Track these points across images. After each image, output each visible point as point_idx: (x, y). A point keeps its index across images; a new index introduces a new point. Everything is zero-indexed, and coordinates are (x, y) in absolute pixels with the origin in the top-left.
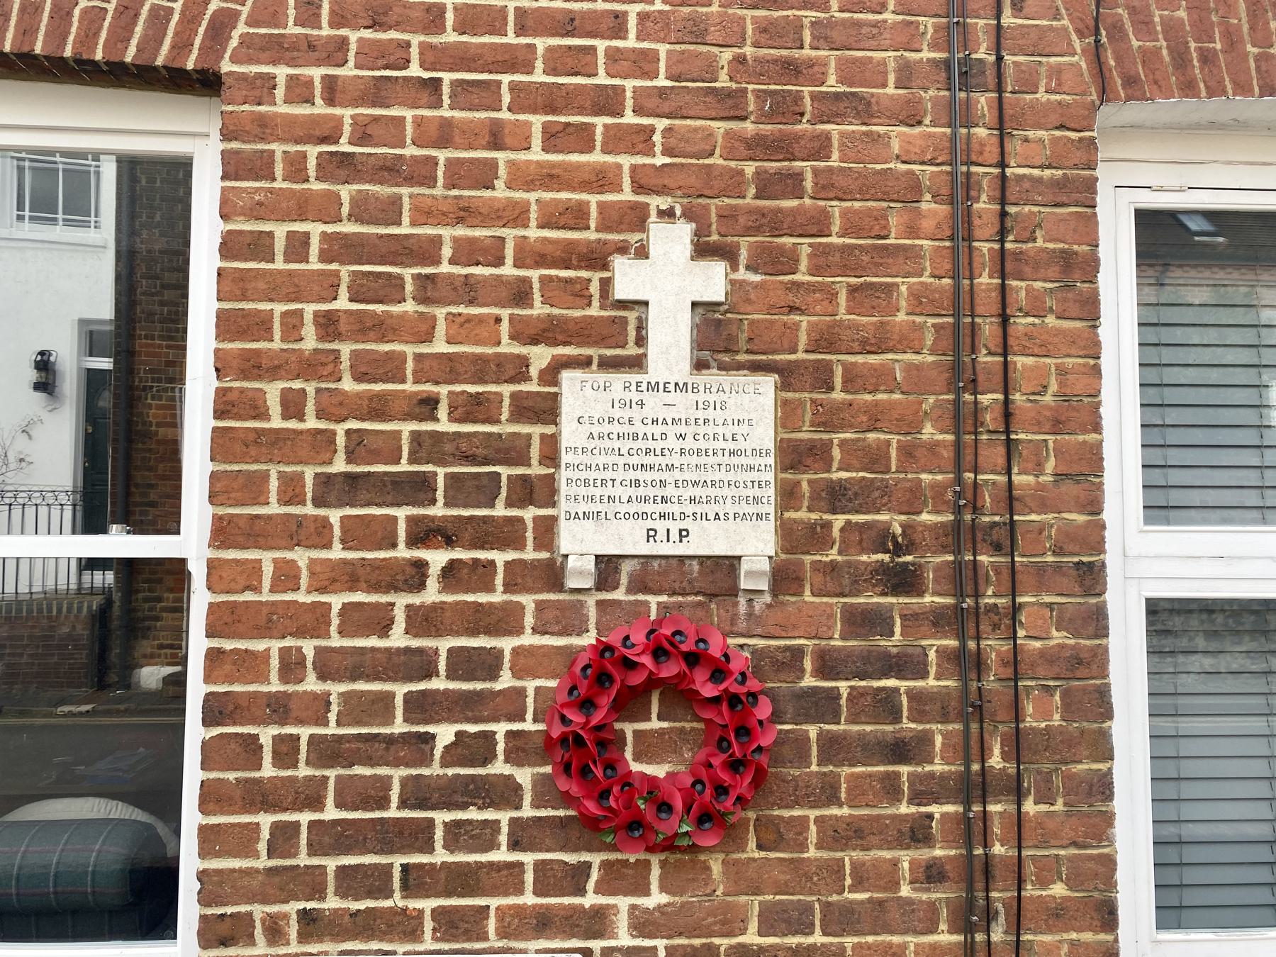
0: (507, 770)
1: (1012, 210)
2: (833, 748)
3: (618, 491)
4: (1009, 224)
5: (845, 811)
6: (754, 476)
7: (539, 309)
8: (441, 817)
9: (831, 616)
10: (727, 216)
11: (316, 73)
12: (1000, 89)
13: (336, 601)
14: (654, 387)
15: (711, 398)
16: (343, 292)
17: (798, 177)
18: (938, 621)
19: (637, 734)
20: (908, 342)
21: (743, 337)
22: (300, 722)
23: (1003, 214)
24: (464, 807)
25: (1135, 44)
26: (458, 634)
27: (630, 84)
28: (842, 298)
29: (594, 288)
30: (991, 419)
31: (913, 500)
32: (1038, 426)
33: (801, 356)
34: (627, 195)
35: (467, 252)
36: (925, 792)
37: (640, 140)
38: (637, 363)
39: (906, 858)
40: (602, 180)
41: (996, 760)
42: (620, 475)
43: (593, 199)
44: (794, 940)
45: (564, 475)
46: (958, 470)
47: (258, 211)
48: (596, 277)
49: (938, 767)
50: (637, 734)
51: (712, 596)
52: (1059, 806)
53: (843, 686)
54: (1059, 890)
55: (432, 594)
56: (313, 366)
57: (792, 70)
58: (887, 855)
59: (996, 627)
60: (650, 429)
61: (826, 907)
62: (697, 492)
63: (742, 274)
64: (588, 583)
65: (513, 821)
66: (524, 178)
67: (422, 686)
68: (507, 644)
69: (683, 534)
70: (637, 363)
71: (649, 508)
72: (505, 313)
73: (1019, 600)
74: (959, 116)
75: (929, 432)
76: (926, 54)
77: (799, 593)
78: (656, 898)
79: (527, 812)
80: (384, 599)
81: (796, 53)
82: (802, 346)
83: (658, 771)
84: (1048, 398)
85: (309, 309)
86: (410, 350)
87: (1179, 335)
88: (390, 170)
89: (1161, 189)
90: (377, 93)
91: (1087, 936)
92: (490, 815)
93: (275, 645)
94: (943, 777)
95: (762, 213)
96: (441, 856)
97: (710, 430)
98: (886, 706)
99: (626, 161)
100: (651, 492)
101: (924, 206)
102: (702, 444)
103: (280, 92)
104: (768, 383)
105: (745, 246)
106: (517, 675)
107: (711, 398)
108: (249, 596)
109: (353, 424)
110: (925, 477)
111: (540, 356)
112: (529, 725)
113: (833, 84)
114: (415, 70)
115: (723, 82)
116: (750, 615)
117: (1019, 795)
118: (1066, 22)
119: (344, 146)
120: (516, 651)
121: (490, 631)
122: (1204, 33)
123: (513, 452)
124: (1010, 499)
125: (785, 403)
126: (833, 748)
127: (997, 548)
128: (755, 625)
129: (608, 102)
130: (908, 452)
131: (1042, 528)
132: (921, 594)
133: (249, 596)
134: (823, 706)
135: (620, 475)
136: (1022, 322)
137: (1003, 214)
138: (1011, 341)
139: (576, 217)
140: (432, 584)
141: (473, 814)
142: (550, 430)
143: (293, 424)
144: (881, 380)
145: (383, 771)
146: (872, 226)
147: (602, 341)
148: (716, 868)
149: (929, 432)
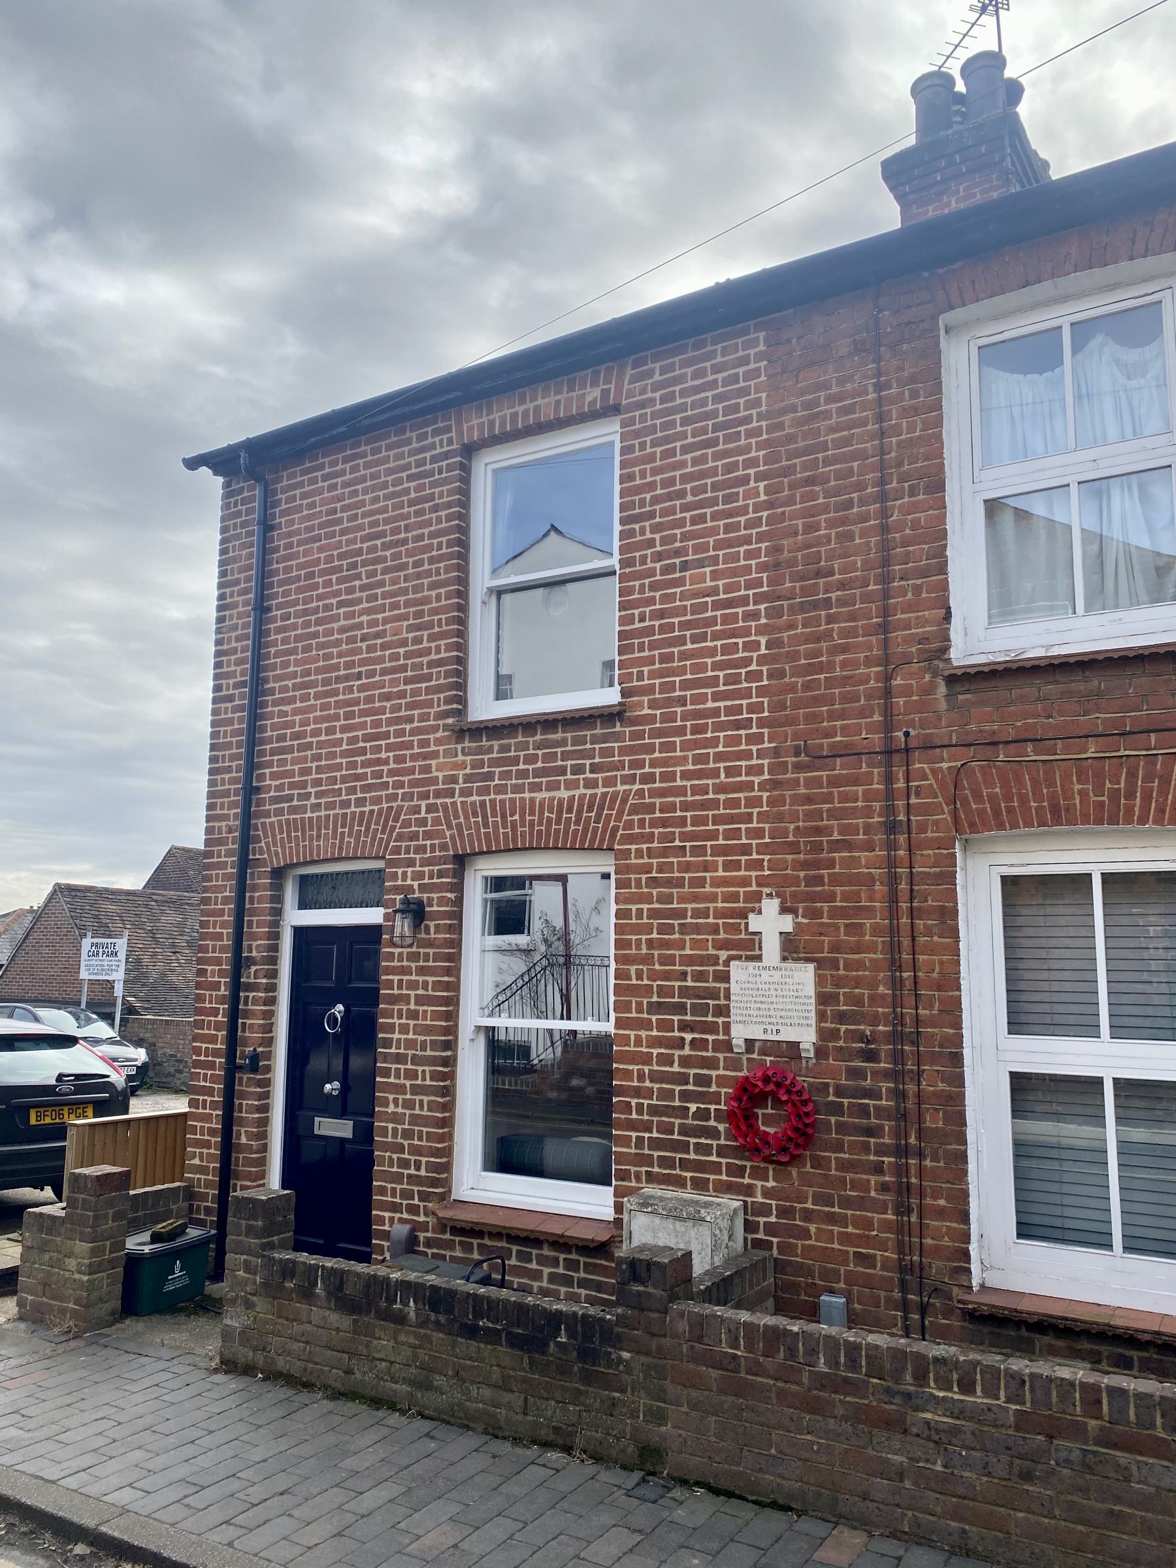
0: (715, 1124)
1: (916, 888)
2: (842, 1128)
3: (752, 1012)
4: (915, 894)
5: (847, 1156)
6: (806, 1007)
7: (722, 936)
8: (693, 1140)
9: (841, 1070)
10: (794, 895)
11: (644, 846)
12: (909, 833)
13: (655, 1052)
14: (765, 968)
15: (788, 973)
16: (655, 931)
17: (822, 877)
18: (886, 1075)
19: (763, 1114)
20: (871, 948)
21: (801, 946)
22: (644, 1098)
23: (912, 890)
24: (700, 1137)
25: (974, 806)
26: (696, 1068)
27: (754, 842)
28: (842, 929)
29: (742, 927)
30: (908, 984)
31: (874, 1020)
32: (930, 988)
33: (825, 955)
34: (754, 888)
35: (697, 914)
36: (881, 1150)
37: (757, 865)
38: (759, 958)
39: (873, 1179)
40: (745, 882)
41: (912, 1140)
42: (753, 1005)
43: (742, 890)
44: (827, 1209)
45: (732, 1005)
46: (894, 1008)
47: (628, 900)
48: (743, 922)
49: (887, 1140)
50: (763, 1114)
51: (792, 1059)
52: (942, 1164)
53: (846, 1101)
54: (942, 1202)
55: (687, 1051)
56: (647, 960)
57: (818, 831)
58: (864, 1177)
59: (912, 1079)
60: (764, 986)
61: (839, 1196)
62: (783, 1013)
63: (800, 919)
64: (743, 1050)
65: (718, 1145)
66: (717, 883)
67: (685, 1088)
68: (714, 1073)
69: (778, 1031)
70: (759, 958)
71: (764, 1020)
72: (710, 937)
73: (923, 1068)
74: (891, 846)
75: (881, 989)
76: (876, 819)
77: (827, 1059)
78: (771, 1184)
79: (723, 1142)
80: (671, 1052)
81: (820, 823)
82: (826, 949)
83: (771, 1130)
84: (935, 975)
85: (644, 937)
86: (677, 953)
87: (1054, 942)
88: (669, 883)
89: (1012, 865)
90: (665, 852)
91: (955, 1225)
92: (709, 1142)
93: (636, 1067)
94: (888, 1145)
95: (807, 893)
96: (692, 1156)
97: (787, 987)
98: (864, 1111)
99: (753, 874)
100: (765, 1013)
101: (876, 888)
102: (785, 993)
103: (633, 855)
104: (811, 967)
105: (801, 908)
106: (718, 1086)
107: (788, 973)
108: (627, 1048)
109: (659, 983)
110: (880, 1010)
111: (723, 955)
112: (723, 1107)
113: (836, 836)
114: (677, 843)
115: (791, 838)
116: (807, 1068)
117: (921, 1155)
118: (940, 799)
119: (654, 875)
120: (717, 1076)
121: (709, 1068)
122: (1008, 798)
123: (714, 994)
124: (917, 1021)
125: (819, 975)
126: (842, 1128)
127: (912, 1043)
128: (809, 1072)
129: (746, 850)
130: (872, 998)
131: (933, 1035)
132: (879, 1062)
133: (627, 1048)
134: (837, 1109)
135: (753, 1005)
136: (922, 939)
137: (912, 890)
138: (917, 949)
139: (734, 897)
140: (687, 1047)
141: (703, 1141)
142: (727, 986)
143: (639, 982)
144: (860, 965)
145: (672, 1120)
146: (854, 897)
147: (745, 949)
148: (794, 1174)
149: (881, 989)
